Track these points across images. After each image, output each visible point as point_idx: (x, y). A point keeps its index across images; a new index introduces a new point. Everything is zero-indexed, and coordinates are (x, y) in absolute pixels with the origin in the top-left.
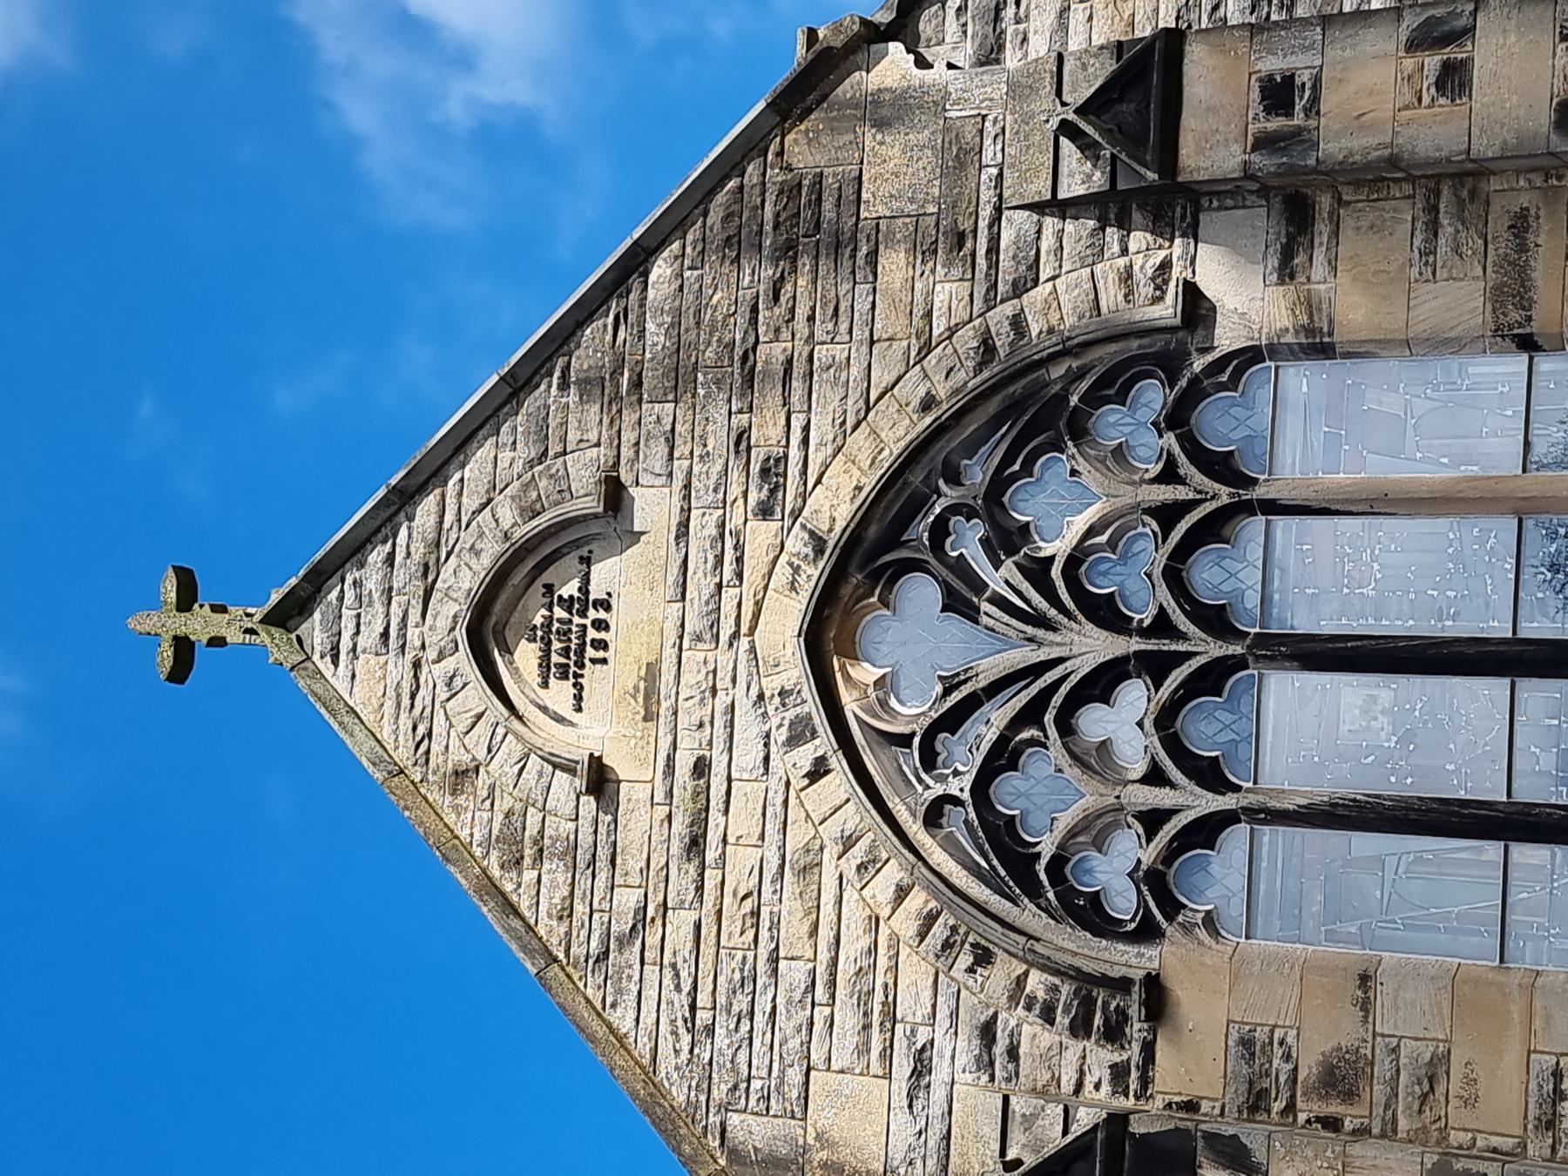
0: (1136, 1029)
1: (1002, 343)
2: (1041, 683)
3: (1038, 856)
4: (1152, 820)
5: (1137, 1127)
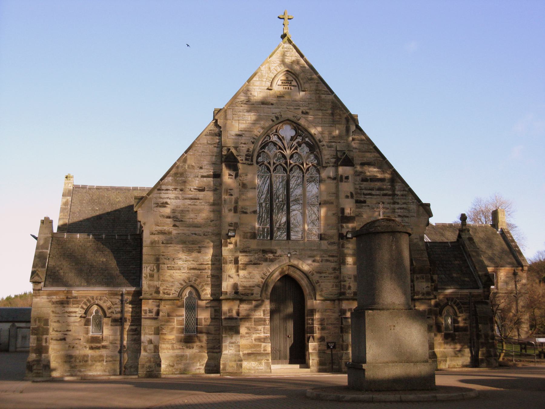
0: (247, 162)
1: (321, 143)
2: (283, 148)
3: (264, 149)
4: (269, 163)
5: (238, 164)
